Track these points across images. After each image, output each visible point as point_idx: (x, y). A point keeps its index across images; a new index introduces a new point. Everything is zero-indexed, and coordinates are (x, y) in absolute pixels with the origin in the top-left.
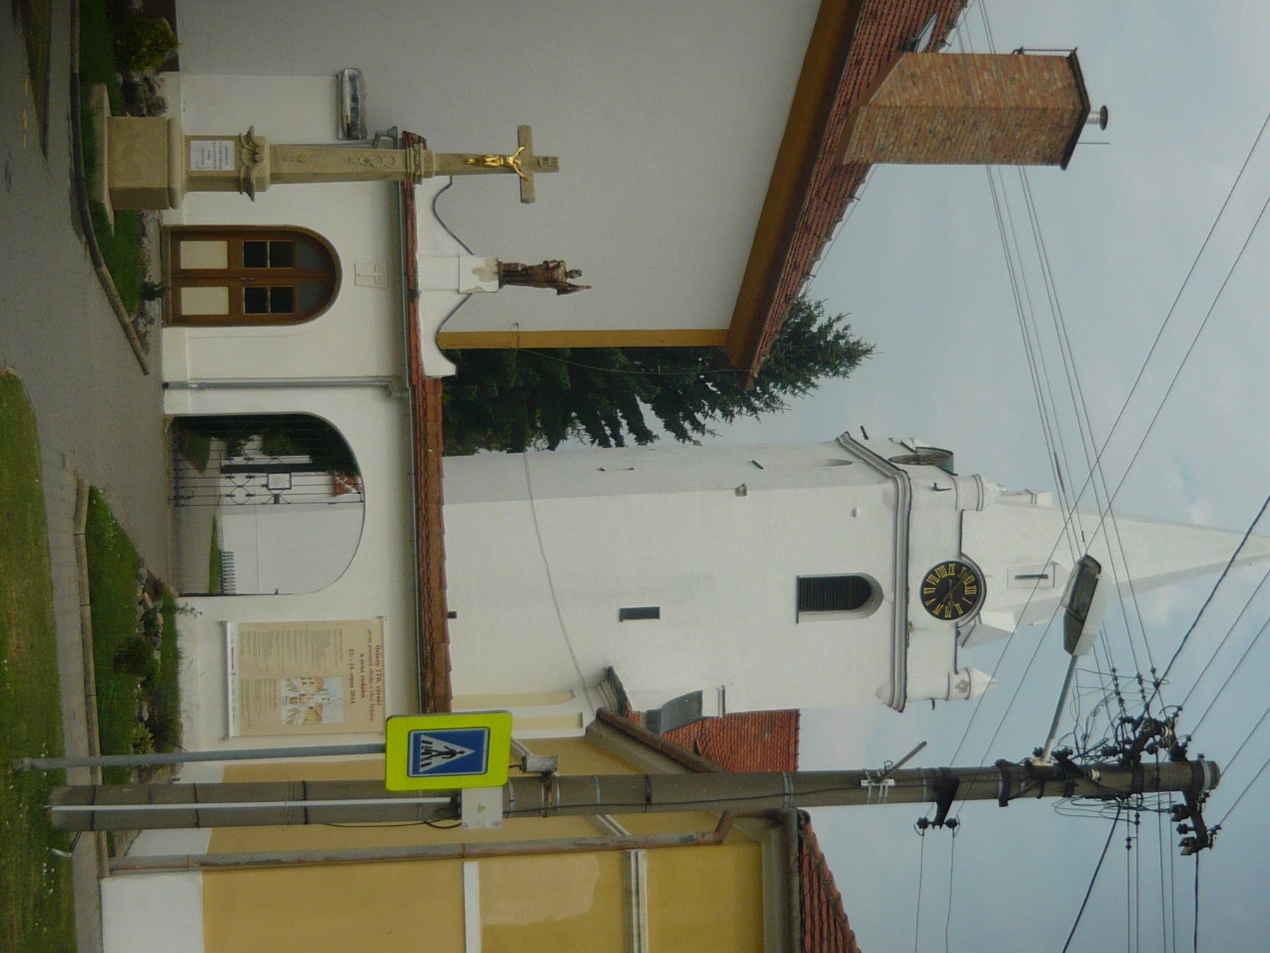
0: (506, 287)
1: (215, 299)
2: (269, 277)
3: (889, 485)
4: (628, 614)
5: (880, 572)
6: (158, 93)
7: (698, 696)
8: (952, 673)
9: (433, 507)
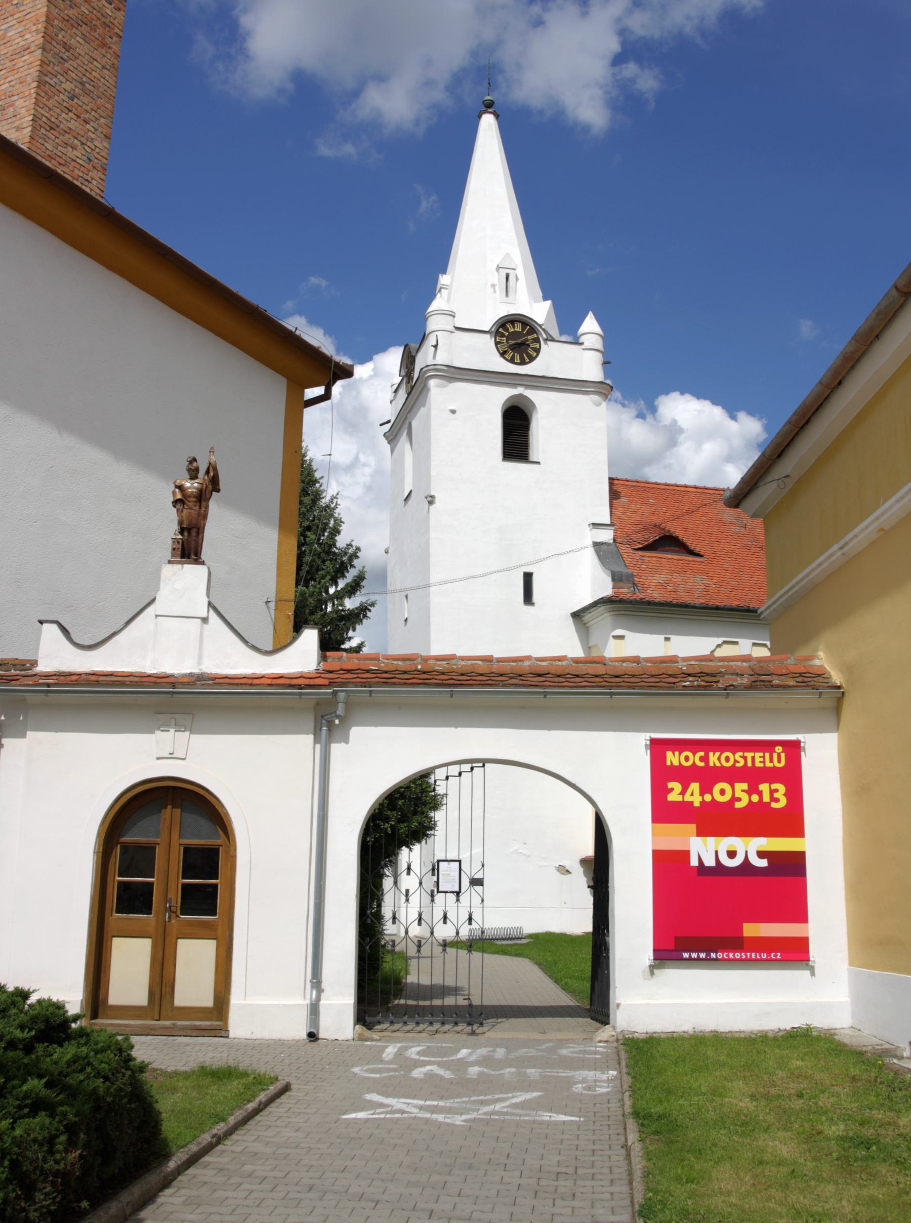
0: (204, 556)
1: (194, 957)
2: (167, 879)
3: (432, 383)
4: (528, 597)
5: (500, 395)
7: (597, 545)
8: (583, 347)
9: (496, 668)
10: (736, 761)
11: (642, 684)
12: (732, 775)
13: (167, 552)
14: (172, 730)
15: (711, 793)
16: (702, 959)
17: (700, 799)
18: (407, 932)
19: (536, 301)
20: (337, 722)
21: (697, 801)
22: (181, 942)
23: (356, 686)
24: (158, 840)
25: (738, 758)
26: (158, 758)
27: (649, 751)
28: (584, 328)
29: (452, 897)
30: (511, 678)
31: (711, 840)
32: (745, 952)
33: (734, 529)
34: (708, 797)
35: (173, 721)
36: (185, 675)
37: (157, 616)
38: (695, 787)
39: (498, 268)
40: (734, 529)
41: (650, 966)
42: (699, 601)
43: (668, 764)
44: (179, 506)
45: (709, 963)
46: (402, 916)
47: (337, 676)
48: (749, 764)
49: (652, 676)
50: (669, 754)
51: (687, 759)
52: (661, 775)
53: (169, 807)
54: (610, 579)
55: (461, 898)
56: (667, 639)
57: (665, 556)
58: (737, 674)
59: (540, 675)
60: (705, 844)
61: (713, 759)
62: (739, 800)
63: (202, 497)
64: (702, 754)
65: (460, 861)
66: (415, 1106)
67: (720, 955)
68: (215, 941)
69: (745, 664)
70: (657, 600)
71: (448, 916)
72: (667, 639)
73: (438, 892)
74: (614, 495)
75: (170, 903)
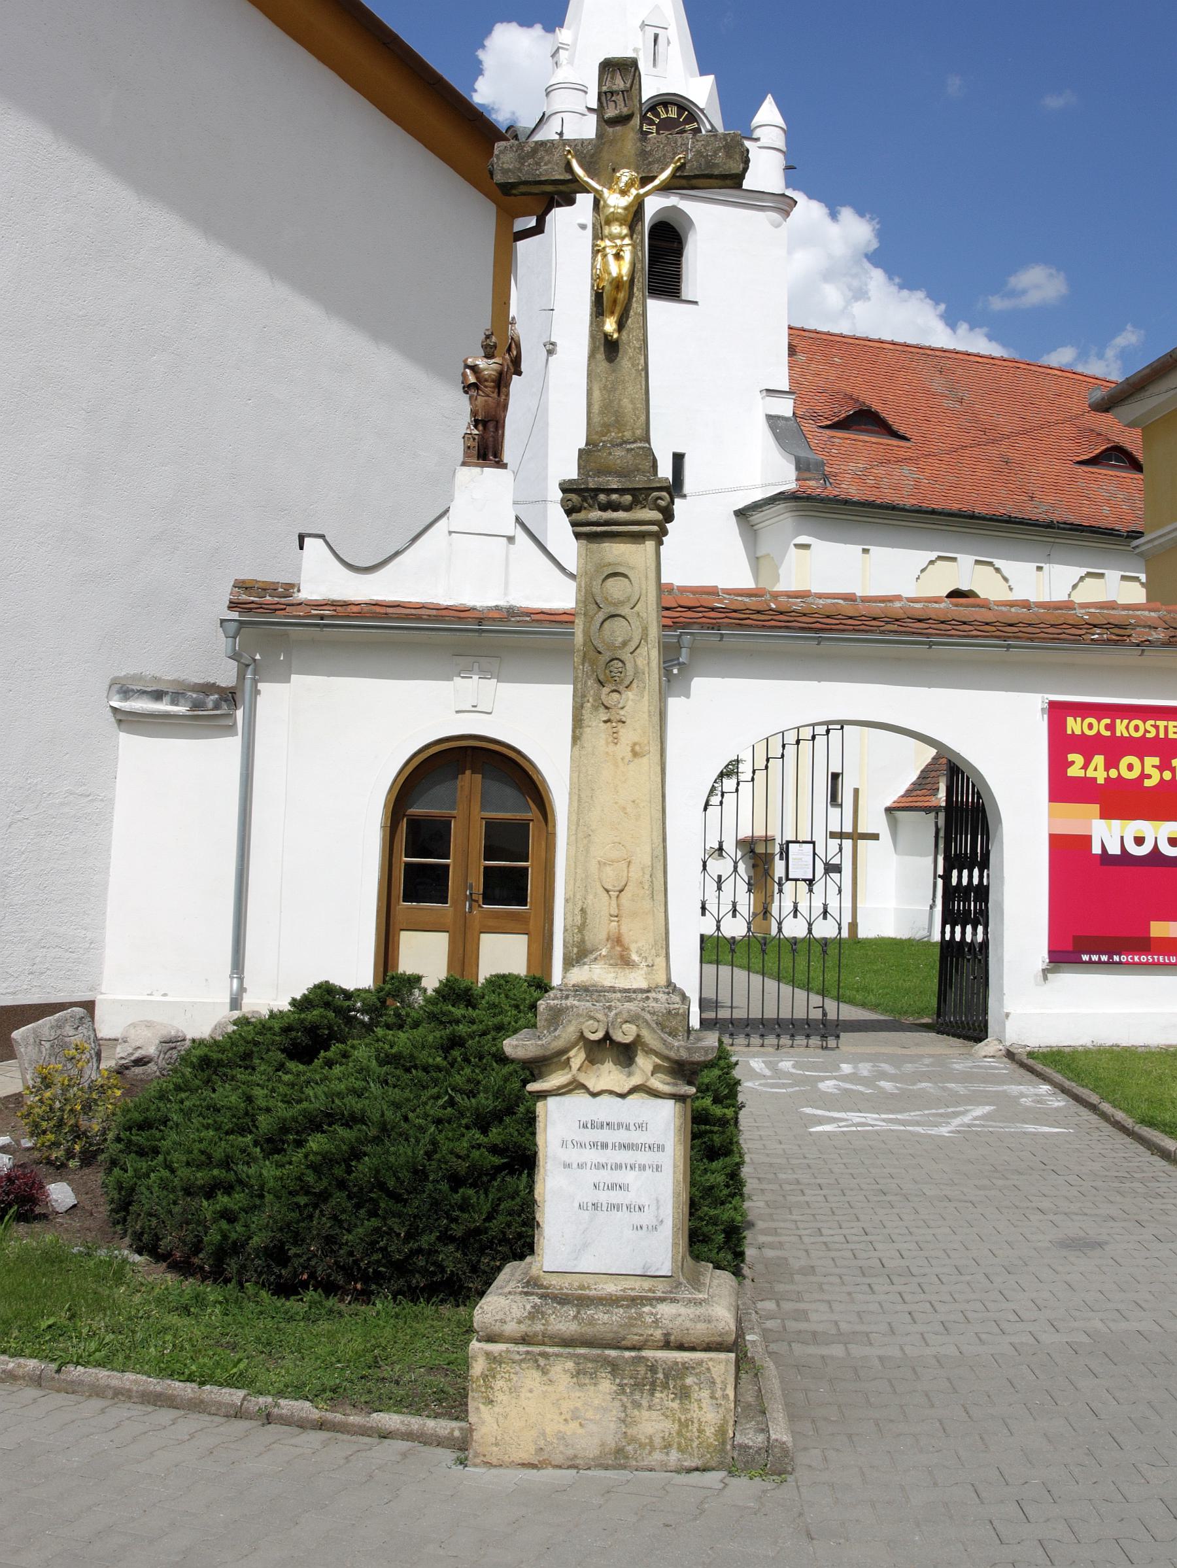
0: (507, 457)
2: (466, 862)
6: (151, 1050)
7: (772, 420)
8: (759, 144)
9: (863, 609)
10: (1146, 731)
11: (1042, 635)
12: (1141, 747)
13: (458, 450)
14: (475, 677)
15: (1118, 769)
16: (1104, 963)
17: (1105, 775)
18: (780, 930)
19: (692, 76)
20: (675, 671)
21: (1101, 777)
22: (484, 938)
23: (702, 628)
24: (454, 813)
25: (1149, 728)
26: (457, 712)
27: (1046, 717)
28: (758, 119)
29: (803, 886)
30: (887, 623)
31: (1116, 823)
32: (1153, 955)
33: (946, 403)
34: (1113, 773)
35: (476, 665)
36: (490, 609)
37: (450, 533)
38: (1099, 760)
39: (644, 25)
40: (946, 403)
41: (1043, 970)
42: (909, 502)
43: (1069, 732)
44: (473, 392)
45: (1111, 966)
46: (803, 907)
47: (678, 614)
48: (1162, 735)
49: (1052, 626)
50: (1070, 720)
51: (1090, 726)
52: (1061, 745)
53: (468, 772)
54: (793, 467)
55: (815, 888)
56: (866, 551)
57: (862, 437)
58: (1150, 627)
59: (920, 621)
60: (1110, 828)
61: (1121, 727)
62: (1149, 777)
63: (501, 383)
64: (1108, 721)
65: (814, 843)
66: (884, 1120)
67: (1124, 958)
68: (446, 935)
69: (1153, 614)
70: (855, 499)
71: (707, 906)
72: (866, 551)
73: (788, 879)
74: (792, 350)
75: (471, 889)
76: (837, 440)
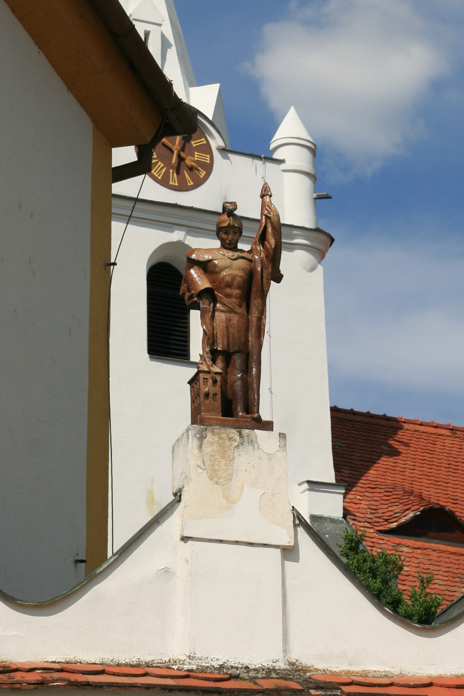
8: (283, 166)
37: (185, 539)
57: (434, 545)
76: (406, 549)
